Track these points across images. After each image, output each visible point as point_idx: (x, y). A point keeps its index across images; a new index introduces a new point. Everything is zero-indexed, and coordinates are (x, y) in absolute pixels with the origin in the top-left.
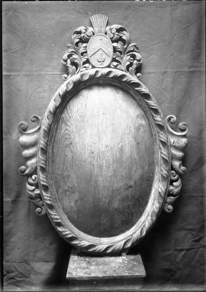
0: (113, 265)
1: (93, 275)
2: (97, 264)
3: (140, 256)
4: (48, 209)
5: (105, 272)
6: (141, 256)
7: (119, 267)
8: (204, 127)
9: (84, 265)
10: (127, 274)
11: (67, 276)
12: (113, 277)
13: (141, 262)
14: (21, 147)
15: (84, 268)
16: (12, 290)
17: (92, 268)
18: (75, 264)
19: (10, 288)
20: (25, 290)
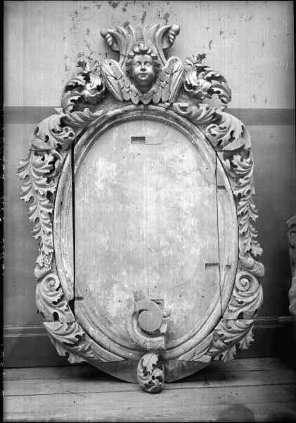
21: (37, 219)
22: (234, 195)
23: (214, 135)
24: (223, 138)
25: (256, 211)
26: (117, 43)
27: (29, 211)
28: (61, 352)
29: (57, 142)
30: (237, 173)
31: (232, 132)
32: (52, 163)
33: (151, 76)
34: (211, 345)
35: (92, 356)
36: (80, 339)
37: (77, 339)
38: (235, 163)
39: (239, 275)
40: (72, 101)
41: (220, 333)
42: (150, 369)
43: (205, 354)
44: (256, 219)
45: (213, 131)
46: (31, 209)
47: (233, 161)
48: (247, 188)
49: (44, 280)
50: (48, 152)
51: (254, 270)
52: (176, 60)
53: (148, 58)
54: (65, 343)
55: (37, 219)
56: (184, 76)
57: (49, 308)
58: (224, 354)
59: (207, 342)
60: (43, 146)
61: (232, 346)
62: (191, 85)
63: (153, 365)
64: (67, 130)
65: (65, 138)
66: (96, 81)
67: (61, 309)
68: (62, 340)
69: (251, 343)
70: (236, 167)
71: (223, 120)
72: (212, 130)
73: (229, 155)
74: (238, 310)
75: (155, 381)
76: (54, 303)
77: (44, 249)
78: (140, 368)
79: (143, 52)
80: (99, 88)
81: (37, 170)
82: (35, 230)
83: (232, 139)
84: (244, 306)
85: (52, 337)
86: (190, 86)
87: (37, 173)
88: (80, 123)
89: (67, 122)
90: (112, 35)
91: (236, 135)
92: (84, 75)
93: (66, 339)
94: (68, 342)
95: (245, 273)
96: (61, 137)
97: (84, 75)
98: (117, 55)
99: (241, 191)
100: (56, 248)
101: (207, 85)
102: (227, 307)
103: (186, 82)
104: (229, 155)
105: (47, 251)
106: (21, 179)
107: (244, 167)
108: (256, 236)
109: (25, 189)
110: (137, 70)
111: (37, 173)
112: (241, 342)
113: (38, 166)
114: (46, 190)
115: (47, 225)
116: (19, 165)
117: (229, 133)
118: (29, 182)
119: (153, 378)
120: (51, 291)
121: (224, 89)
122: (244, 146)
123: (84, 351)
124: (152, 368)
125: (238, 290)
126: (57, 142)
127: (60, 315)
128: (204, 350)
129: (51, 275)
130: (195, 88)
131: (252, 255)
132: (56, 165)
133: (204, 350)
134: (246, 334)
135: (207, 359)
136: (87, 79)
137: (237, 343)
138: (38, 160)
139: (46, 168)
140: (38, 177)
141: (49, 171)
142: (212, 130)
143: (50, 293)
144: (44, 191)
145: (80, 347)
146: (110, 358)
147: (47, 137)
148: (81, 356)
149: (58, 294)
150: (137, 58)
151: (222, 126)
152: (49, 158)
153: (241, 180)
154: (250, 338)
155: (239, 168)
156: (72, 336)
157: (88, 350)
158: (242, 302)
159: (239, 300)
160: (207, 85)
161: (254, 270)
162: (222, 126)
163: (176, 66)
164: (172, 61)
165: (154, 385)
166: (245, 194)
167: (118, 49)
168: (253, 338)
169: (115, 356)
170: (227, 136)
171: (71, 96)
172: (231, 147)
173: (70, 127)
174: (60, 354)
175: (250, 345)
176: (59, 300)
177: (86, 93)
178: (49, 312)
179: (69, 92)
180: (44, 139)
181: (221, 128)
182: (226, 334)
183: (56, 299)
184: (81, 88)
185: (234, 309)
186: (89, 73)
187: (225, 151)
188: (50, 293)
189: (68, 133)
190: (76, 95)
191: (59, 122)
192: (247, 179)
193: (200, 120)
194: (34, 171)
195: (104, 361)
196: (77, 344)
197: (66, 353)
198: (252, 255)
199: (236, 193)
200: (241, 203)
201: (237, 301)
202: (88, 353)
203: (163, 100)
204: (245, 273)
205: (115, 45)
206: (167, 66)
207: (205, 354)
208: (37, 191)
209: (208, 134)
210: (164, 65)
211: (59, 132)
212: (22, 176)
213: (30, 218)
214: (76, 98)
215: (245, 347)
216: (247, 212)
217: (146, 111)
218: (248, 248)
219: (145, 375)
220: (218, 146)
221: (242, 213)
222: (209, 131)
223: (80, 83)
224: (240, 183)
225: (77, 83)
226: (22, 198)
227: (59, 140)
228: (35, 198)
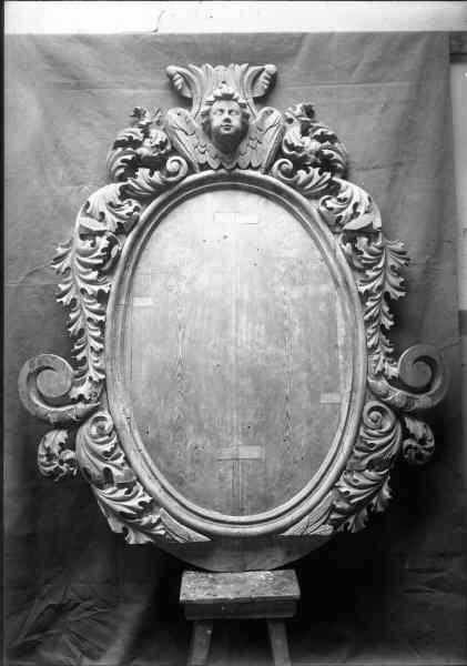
0: (252, 583)
1: (219, 597)
2: (226, 583)
3: (293, 572)
4: (386, 484)
5: (238, 593)
6: (297, 574)
7: (260, 585)
8: (11, 572)
9: (206, 583)
10: (272, 595)
11: (181, 598)
12: (251, 598)
13: (295, 578)
14: (457, 313)
15: (205, 588)
16: (7, 444)
17: (219, 587)
18: (192, 583)
19: (10, 458)
20: (8, 501)
21: (82, 332)
22: (360, 293)
23: (331, 209)
24: (343, 214)
25: (391, 316)
26: (189, 87)
27: (69, 318)
28: (116, 526)
29: (117, 220)
30: (364, 261)
31: (356, 205)
32: (108, 250)
33: (237, 131)
34: (333, 509)
35: (163, 532)
36: (148, 508)
37: (141, 508)
38: (361, 249)
39: (367, 407)
40: (123, 161)
41: (343, 490)
42: (55, 450)
43: (324, 524)
44: (391, 327)
45: (330, 204)
46: (72, 316)
47: (357, 245)
48: (378, 282)
49: (91, 420)
50: (101, 233)
51: (390, 398)
52: (272, 112)
53: (234, 106)
54: (122, 513)
55: (82, 332)
56: (282, 134)
57: (96, 461)
58: (351, 520)
59: (325, 505)
60: (96, 226)
61: (360, 510)
62: (293, 144)
63: (61, 444)
64: (130, 203)
65: (128, 214)
66: (158, 135)
67: (115, 462)
68: (119, 507)
69: (389, 500)
70: (361, 253)
71: (342, 189)
72: (327, 202)
73: (351, 237)
74: (367, 456)
75: (64, 468)
76: (106, 453)
77: (92, 373)
78: (41, 452)
79: (228, 97)
80: (162, 145)
81: (83, 259)
82: (76, 347)
83: (355, 215)
84: (375, 451)
85: (104, 503)
86: (291, 147)
87: (85, 265)
88: (149, 192)
89: (128, 192)
90: (182, 75)
91: (361, 209)
92: (141, 127)
93: (125, 506)
94: (128, 511)
95: (376, 403)
96: (123, 213)
97: (141, 127)
98: (187, 103)
99: (368, 287)
100: (109, 373)
101: (315, 145)
102: (352, 453)
103: (286, 141)
104: (351, 237)
105: (97, 377)
106: (58, 272)
107: (371, 253)
108: (391, 350)
109: (63, 288)
110: (217, 121)
111: (85, 265)
112: (374, 501)
113: (85, 254)
114: (96, 288)
115: (97, 339)
116: (56, 252)
117: (351, 205)
118: (70, 278)
119: (61, 462)
120: (102, 436)
121: (338, 152)
122: (371, 225)
123: (151, 526)
124: (60, 448)
125: (367, 427)
126: (117, 220)
127: (116, 472)
128: (321, 518)
129: (99, 414)
130: (299, 149)
131: (386, 377)
132: (114, 253)
133: (321, 518)
134: (378, 491)
135: (327, 530)
136: (146, 131)
137: (366, 503)
138: (87, 245)
139: (98, 257)
140: (84, 270)
141: (101, 261)
142: (327, 202)
143: (101, 440)
144: (92, 289)
145: (145, 520)
146: (189, 537)
147: (102, 214)
148: (146, 533)
149: (110, 441)
150: (217, 105)
151: (341, 196)
152: (103, 242)
153: (368, 273)
154: (386, 493)
155: (366, 255)
156: (134, 503)
157: (156, 524)
158: (372, 445)
159: (369, 442)
160: (315, 145)
161: (390, 398)
162: (341, 196)
163: (271, 120)
164: (266, 112)
165: (61, 471)
166: (374, 291)
167: (188, 95)
168: (391, 494)
169: (191, 532)
170: (350, 210)
171: (119, 155)
172: (354, 225)
173: (134, 198)
174: (113, 529)
175: (387, 505)
176: (113, 450)
177: (144, 151)
178: (97, 467)
179: (120, 150)
180: (98, 216)
181: (339, 200)
182: (353, 491)
183: (107, 448)
184: (137, 144)
185: (360, 454)
186: (149, 124)
187: (346, 231)
188: (101, 440)
189: (133, 207)
190: (130, 153)
191: (119, 193)
192: (377, 270)
193: (311, 189)
194: (79, 261)
195: (181, 541)
196: (140, 514)
197: (124, 529)
198: (386, 377)
199: (363, 289)
200: (369, 304)
201: (366, 443)
202: (158, 527)
203: (254, 165)
204: (376, 403)
205: (186, 89)
206: (258, 119)
207: (324, 524)
208: (83, 291)
209: (323, 209)
210: (255, 117)
211: (119, 206)
212: (60, 268)
213: (71, 329)
214: (129, 157)
215: (380, 509)
216: (378, 316)
217: (231, 181)
218: (379, 368)
219: (49, 460)
220: (336, 224)
221: (371, 317)
222: (324, 203)
223: (135, 138)
224: (367, 276)
225: (131, 138)
226: (58, 300)
227: (120, 217)
228: (79, 302)
